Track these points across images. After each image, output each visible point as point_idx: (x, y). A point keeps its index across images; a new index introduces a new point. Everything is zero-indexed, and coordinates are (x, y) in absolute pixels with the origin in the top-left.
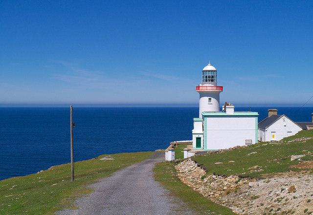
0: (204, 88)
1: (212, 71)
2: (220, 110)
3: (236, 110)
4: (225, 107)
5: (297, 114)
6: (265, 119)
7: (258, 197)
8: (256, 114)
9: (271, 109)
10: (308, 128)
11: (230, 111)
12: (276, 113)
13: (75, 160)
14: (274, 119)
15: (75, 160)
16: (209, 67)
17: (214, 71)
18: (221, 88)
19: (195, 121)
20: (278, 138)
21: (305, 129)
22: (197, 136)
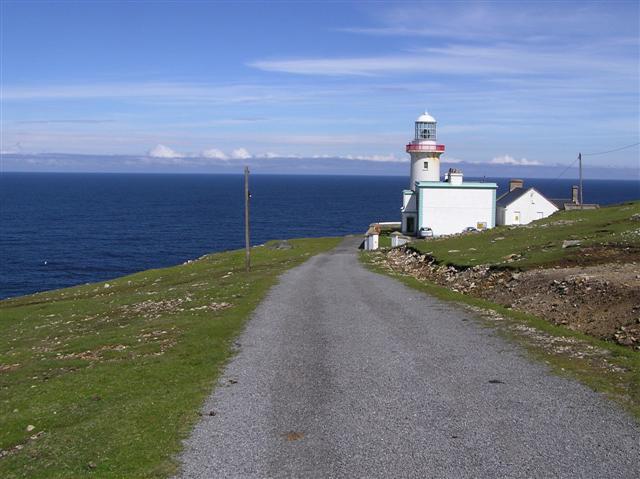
0: (424, 148)
1: (430, 123)
2: (442, 179)
3: (465, 180)
4: (449, 176)
5: (552, 190)
6: (506, 194)
7: (491, 382)
8: (495, 185)
9: (509, 181)
10: (567, 208)
11: (457, 180)
12: (520, 186)
13: (251, 245)
14: (519, 192)
15: (251, 245)
16: (426, 118)
17: (433, 123)
18: (638, 322)
19: (580, 175)
20: (525, 220)
21: (562, 208)
22: (408, 215)
